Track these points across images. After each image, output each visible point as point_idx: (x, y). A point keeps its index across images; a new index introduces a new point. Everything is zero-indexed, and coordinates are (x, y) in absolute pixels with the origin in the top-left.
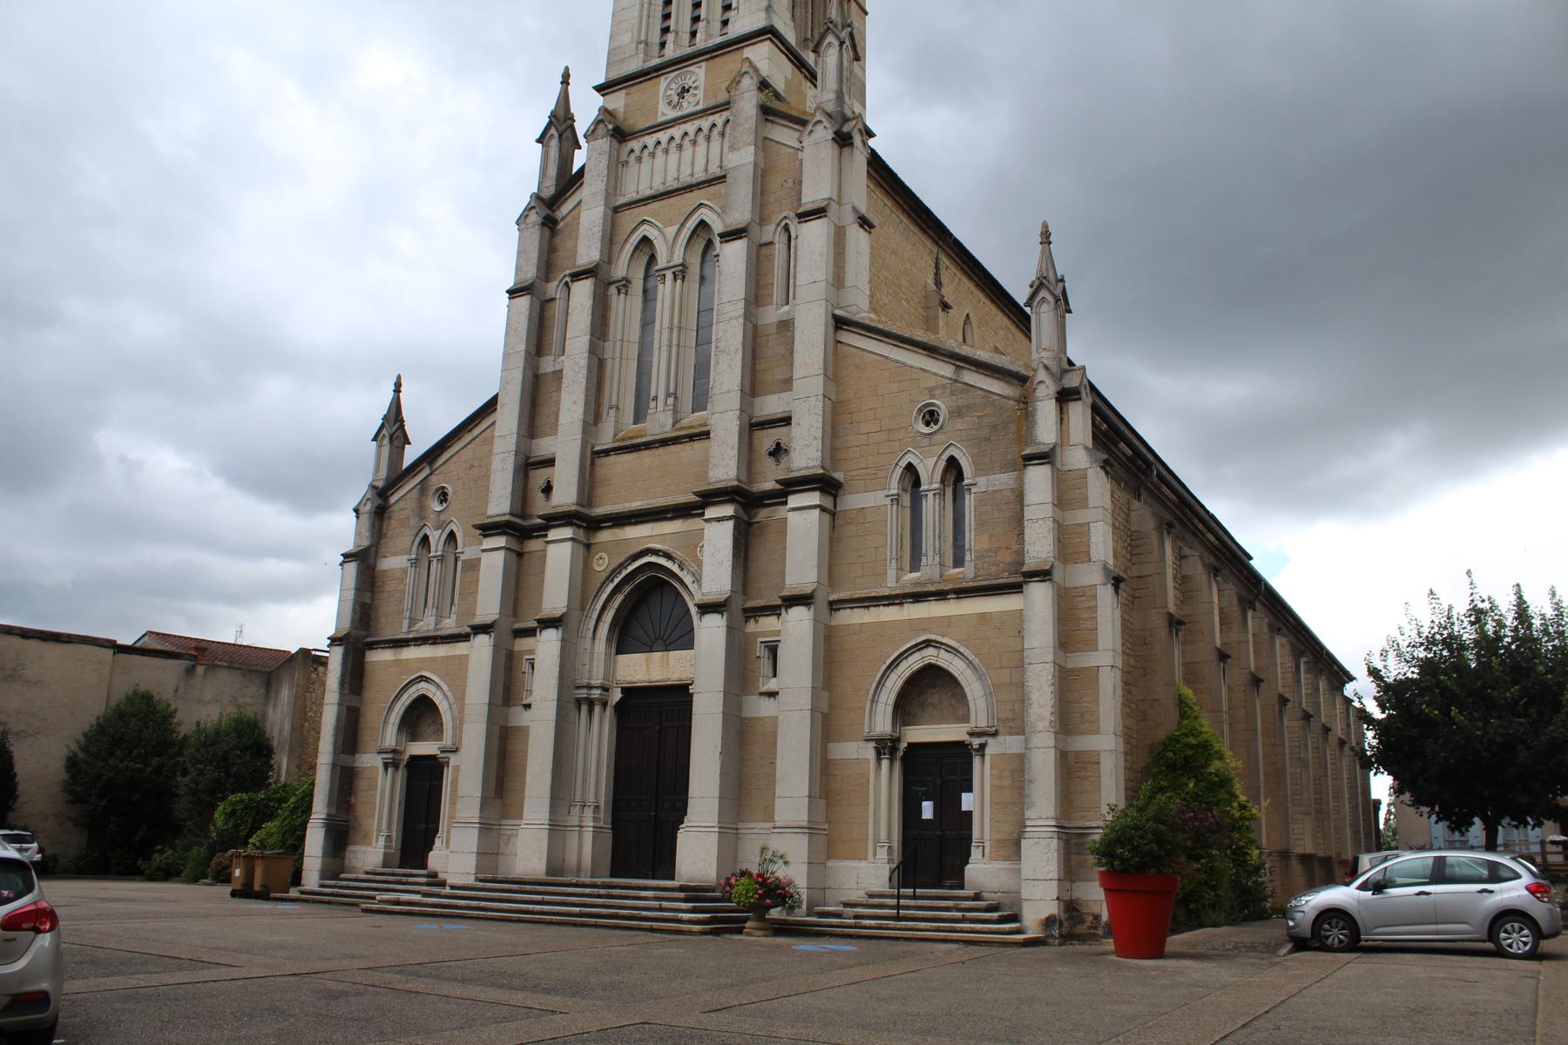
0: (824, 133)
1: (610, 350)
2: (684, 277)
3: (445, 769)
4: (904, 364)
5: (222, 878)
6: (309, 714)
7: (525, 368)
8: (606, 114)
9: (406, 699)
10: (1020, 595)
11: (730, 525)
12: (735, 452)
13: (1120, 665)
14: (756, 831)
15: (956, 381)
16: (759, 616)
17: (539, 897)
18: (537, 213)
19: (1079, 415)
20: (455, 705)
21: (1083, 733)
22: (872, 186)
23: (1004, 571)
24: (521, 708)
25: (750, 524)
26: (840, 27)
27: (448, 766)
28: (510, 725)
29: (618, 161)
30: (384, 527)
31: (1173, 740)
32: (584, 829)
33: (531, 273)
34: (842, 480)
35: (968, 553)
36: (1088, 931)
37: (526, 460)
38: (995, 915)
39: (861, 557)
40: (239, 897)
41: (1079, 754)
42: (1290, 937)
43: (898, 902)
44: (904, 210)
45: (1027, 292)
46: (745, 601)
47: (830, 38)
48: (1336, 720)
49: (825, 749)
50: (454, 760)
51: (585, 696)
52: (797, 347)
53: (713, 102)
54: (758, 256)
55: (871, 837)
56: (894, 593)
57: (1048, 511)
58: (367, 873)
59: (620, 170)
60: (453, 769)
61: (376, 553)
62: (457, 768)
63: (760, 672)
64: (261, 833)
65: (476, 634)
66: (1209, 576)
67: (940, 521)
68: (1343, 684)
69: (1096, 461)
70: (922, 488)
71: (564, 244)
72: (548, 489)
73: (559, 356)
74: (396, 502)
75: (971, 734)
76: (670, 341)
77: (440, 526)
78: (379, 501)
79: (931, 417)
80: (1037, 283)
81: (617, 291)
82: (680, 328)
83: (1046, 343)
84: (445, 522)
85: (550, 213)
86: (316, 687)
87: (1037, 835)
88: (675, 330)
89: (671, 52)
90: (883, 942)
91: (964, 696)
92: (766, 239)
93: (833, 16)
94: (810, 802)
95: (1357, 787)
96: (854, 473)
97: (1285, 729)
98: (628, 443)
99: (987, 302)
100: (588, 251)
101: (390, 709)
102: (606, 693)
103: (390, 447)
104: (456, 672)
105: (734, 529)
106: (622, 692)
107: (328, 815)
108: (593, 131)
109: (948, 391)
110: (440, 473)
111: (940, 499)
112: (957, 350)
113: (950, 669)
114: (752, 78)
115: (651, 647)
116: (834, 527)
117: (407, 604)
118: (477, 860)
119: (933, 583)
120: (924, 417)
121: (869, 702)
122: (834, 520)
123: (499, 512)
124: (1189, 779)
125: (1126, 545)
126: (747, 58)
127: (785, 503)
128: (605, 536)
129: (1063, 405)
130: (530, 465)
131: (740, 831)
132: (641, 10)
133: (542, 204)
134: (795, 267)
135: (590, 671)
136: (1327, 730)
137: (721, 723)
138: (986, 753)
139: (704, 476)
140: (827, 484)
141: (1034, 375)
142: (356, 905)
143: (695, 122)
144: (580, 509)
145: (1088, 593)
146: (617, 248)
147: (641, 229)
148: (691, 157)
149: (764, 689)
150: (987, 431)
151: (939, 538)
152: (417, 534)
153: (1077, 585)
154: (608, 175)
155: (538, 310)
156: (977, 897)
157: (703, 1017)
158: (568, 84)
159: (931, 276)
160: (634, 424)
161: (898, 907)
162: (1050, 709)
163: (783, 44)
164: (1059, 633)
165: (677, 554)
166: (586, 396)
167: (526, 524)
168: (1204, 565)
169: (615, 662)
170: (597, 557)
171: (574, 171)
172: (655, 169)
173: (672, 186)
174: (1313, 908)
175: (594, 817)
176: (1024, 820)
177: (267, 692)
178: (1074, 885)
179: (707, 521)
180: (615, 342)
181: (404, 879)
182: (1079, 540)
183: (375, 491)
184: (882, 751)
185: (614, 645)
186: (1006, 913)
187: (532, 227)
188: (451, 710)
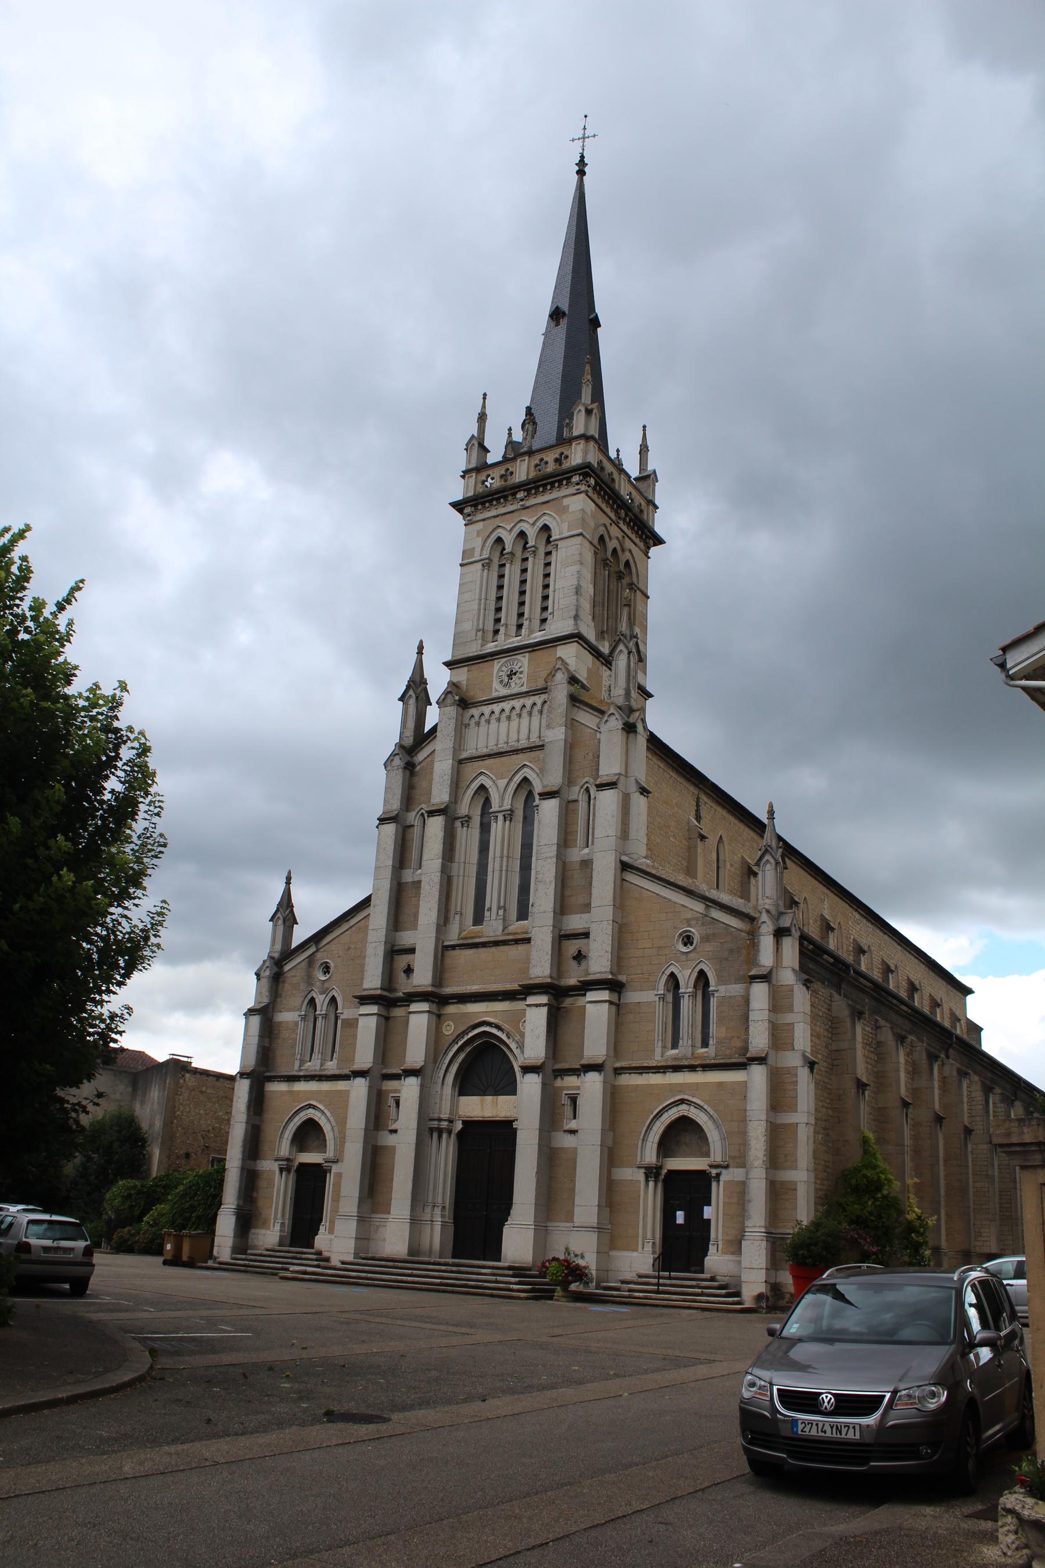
0: (615, 723)
1: (456, 869)
2: (511, 819)
3: (328, 1175)
4: (670, 900)
5: (123, 1248)
9: (298, 1121)
11: (545, 1010)
12: (549, 957)
14: (559, 1228)
15: (706, 916)
16: (564, 1075)
17: (410, 1271)
19: (790, 948)
21: (785, 1169)
22: (650, 757)
24: (387, 1132)
25: (559, 1009)
26: (628, 638)
27: (330, 1173)
28: (379, 1144)
30: (280, 989)
31: (857, 1170)
32: (434, 1223)
33: (396, 805)
34: (624, 981)
35: (711, 1039)
37: (392, 948)
38: (724, 1291)
40: (169, 1265)
41: (783, 1183)
44: (673, 768)
46: (554, 1064)
47: (621, 647)
49: (609, 1172)
50: (335, 1168)
52: (595, 883)
54: (567, 809)
55: (640, 1235)
56: (659, 1064)
57: (765, 1015)
59: (463, 730)
61: (273, 1008)
62: (339, 1175)
64: (153, 1213)
65: (355, 1077)
66: (897, 1044)
67: (692, 1015)
69: (799, 980)
70: (711, 988)
71: (421, 783)
72: (409, 971)
75: (711, 1166)
76: (501, 867)
77: (324, 991)
78: (276, 969)
79: (688, 940)
81: (460, 825)
82: (508, 857)
85: (410, 759)
86: (183, 1091)
87: (752, 1238)
88: (505, 859)
89: (505, 641)
90: (648, 1307)
91: (707, 1139)
94: (599, 1210)
96: (633, 977)
98: (470, 941)
99: (737, 822)
100: (440, 795)
101: (285, 1128)
105: (548, 1013)
107: (238, 1206)
108: (444, 699)
109: (700, 922)
110: (324, 951)
112: (707, 894)
113: (697, 1120)
116: (618, 1014)
117: (298, 1048)
118: (355, 1244)
119: (687, 1059)
120: (683, 940)
121: (640, 1141)
123: (373, 987)
124: (869, 1199)
125: (827, 1027)
126: (560, 657)
127: (585, 995)
128: (452, 1009)
129: (779, 939)
130: (394, 952)
132: (480, 604)
133: (403, 751)
134: (594, 820)
135: (440, 1108)
138: (721, 1179)
139: (526, 970)
140: (615, 986)
141: (759, 917)
142: (276, 1274)
145: (792, 1072)
146: (461, 791)
147: (480, 779)
148: (517, 727)
149: (567, 1128)
150: (727, 953)
152: (306, 997)
154: (455, 736)
156: (713, 1279)
157: (549, 1339)
159: (693, 813)
160: (473, 926)
161: (658, 1285)
163: (586, 644)
164: (771, 1099)
165: (505, 1026)
167: (392, 996)
169: (458, 1102)
170: (446, 1024)
171: (426, 730)
173: (503, 748)
177: (134, 1090)
181: (299, 1256)
183: (272, 961)
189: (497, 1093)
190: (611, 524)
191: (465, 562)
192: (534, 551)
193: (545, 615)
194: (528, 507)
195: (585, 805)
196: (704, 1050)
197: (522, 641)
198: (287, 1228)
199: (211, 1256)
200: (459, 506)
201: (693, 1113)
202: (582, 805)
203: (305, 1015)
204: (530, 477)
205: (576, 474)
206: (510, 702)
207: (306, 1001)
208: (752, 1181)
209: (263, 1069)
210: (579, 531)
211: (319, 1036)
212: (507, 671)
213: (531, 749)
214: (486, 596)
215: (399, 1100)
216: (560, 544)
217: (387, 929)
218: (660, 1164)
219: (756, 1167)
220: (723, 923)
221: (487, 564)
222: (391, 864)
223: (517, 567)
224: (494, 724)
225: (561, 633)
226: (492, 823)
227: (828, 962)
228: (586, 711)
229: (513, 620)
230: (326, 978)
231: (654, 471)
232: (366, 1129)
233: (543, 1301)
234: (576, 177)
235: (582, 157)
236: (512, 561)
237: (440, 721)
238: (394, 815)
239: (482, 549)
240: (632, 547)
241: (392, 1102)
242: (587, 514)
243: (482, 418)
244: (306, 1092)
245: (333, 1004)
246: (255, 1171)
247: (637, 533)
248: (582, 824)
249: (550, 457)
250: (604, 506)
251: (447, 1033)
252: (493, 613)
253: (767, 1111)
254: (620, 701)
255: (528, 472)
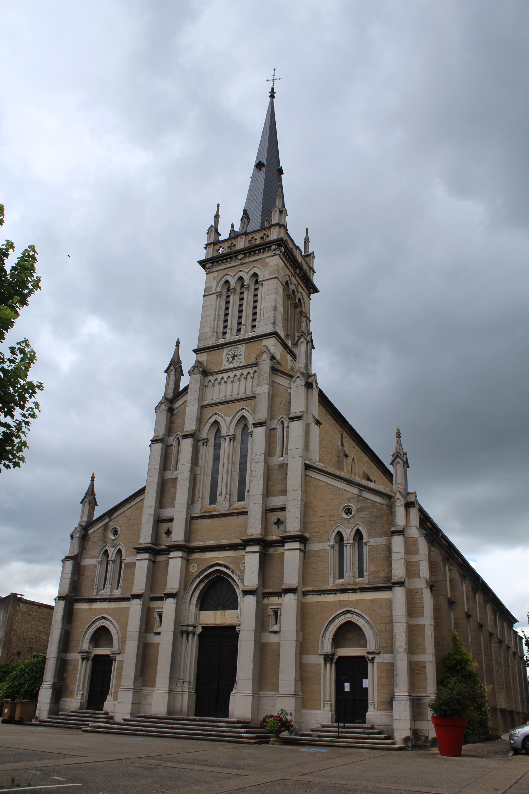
0: (300, 382)
1: (199, 471)
2: (234, 440)
3: (114, 662)
4: (336, 487)
6: (14, 627)
7: (159, 476)
8: (198, 364)
9: (94, 627)
10: (391, 591)
11: (258, 555)
12: (260, 522)
13: (433, 624)
14: (268, 695)
15: (360, 496)
16: (270, 596)
18: (165, 405)
19: (414, 514)
20: (119, 632)
23: (382, 581)
24: (153, 634)
25: (265, 555)
26: (307, 335)
27: (115, 660)
28: (147, 642)
29: (204, 385)
32: (184, 693)
33: (162, 432)
34: (308, 537)
36: (423, 744)
38: (383, 736)
39: (317, 572)
42: (512, 748)
43: (338, 730)
45: (391, 459)
46: (263, 589)
47: (302, 339)
48: (511, 642)
49: (301, 658)
50: (118, 658)
51: (186, 630)
52: (289, 476)
53: (248, 363)
54: (270, 434)
56: (332, 588)
57: (402, 555)
58: (72, 712)
59: (204, 388)
60: (118, 662)
61: (81, 556)
62: (121, 662)
63: (270, 622)
65: (133, 599)
66: (462, 580)
68: (512, 623)
69: (422, 534)
70: (345, 542)
71: (178, 421)
72: (168, 532)
73: (174, 471)
74: (92, 533)
75: (368, 653)
76: (228, 469)
78: (83, 532)
79: (348, 511)
80: (395, 455)
81: (202, 445)
82: (232, 463)
83: (399, 481)
84: (116, 544)
86: (18, 614)
88: (230, 464)
89: (229, 338)
91: (364, 635)
92: (272, 427)
93: (303, 329)
94: (295, 683)
95: (521, 675)
97: (492, 647)
100: (190, 426)
101: (86, 632)
102: (194, 629)
103: (89, 507)
104: (125, 614)
106: (202, 628)
107: (54, 682)
108: (193, 371)
109: (356, 500)
110: (114, 521)
111: (352, 547)
112: (360, 482)
113: (358, 623)
114: (267, 354)
115: (216, 608)
116: (304, 558)
118: (131, 707)
119: (350, 585)
120: (345, 511)
122: (304, 554)
126: (265, 345)
128: (196, 556)
131: (260, 695)
132: (215, 317)
133: (167, 401)
135: (188, 618)
136: (508, 648)
137: (253, 646)
140: (302, 539)
141: (395, 496)
142: (80, 728)
143: (240, 371)
144: (185, 543)
145: (419, 591)
146: (203, 424)
147: (214, 417)
149: (272, 630)
150: (374, 519)
151: (353, 565)
152: (102, 549)
153: (415, 588)
155: (165, 450)
156: (372, 728)
158: (179, 346)
159: (340, 442)
160: (209, 505)
161: (338, 732)
162: (404, 643)
163: (280, 339)
164: (407, 609)
165: (231, 566)
166: (189, 492)
168: (459, 574)
169: (199, 614)
170: (192, 565)
171: (180, 390)
172: (220, 390)
173: (229, 398)
174: (522, 735)
175: (188, 687)
176: (394, 693)
178: (416, 722)
179: (247, 552)
180: (201, 467)
181: (93, 715)
182: (415, 568)
183: (81, 527)
184: (327, 660)
185: (199, 606)
186: (386, 735)
187: (163, 412)
188: (118, 634)
189: (224, 609)
190: (292, 276)
191: (206, 294)
192: (248, 288)
193: (254, 323)
194: (244, 264)
195: (281, 431)
196: (360, 579)
197: (241, 337)
198: (86, 698)
199: (33, 716)
200: (202, 263)
201: (355, 619)
202: (279, 431)
203: (101, 561)
204: (245, 247)
205: (273, 245)
206: (233, 372)
207: (102, 552)
208: (398, 661)
209: (73, 594)
210: (276, 276)
211: (109, 574)
212: (232, 354)
213: (247, 399)
214: (219, 313)
215: (162, 613)
216: (264, 283)
217: (155, 507)
218: (333, 652)
219: (400, 653)
220: (371, 500)
221: (219, 295)
222: (159, 467)
223: (237, 297)
224: (223, 385)
225: (265, 332)
226: (222, 442)
227: (428, 527)
228: (281, 376)
229: (235, 326)
230: (115, 538)
231: (313, 253)
232: (140, 632)
233: (264, 745)
234: (269, 99)
235: (273, 89)
236: (234, 294)
237: (190, 383)
238: (161, 438)
239: (217, 287)
240: (302, 291)
241: (156, 615)
242: (280, 267)
243: (217, 217)
244: (100, 609)
245: (119, 554)
246: (66, 659)
247: (304, 284)
248: (279, 442)
249: (258, 236)
250: (288, 265)
251: (192, 571)
252: (223, 322)
253: (406, 616)
254: (303, 370)
255: (245, 245)
